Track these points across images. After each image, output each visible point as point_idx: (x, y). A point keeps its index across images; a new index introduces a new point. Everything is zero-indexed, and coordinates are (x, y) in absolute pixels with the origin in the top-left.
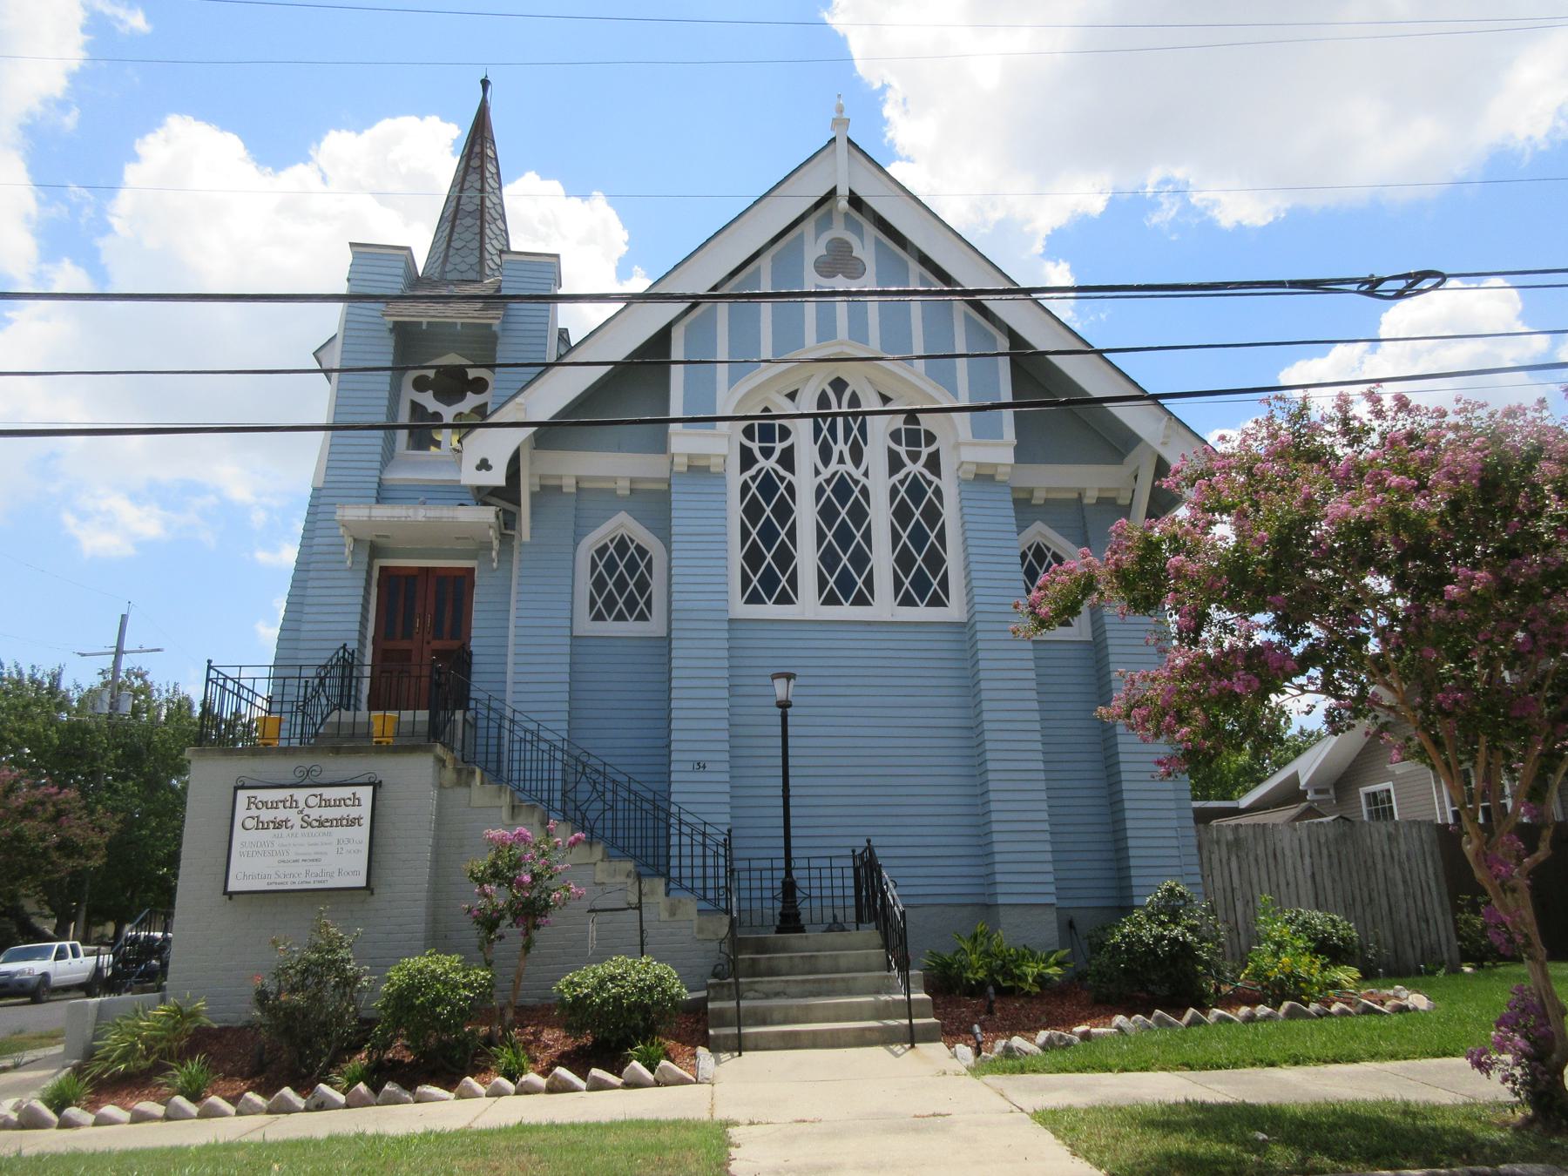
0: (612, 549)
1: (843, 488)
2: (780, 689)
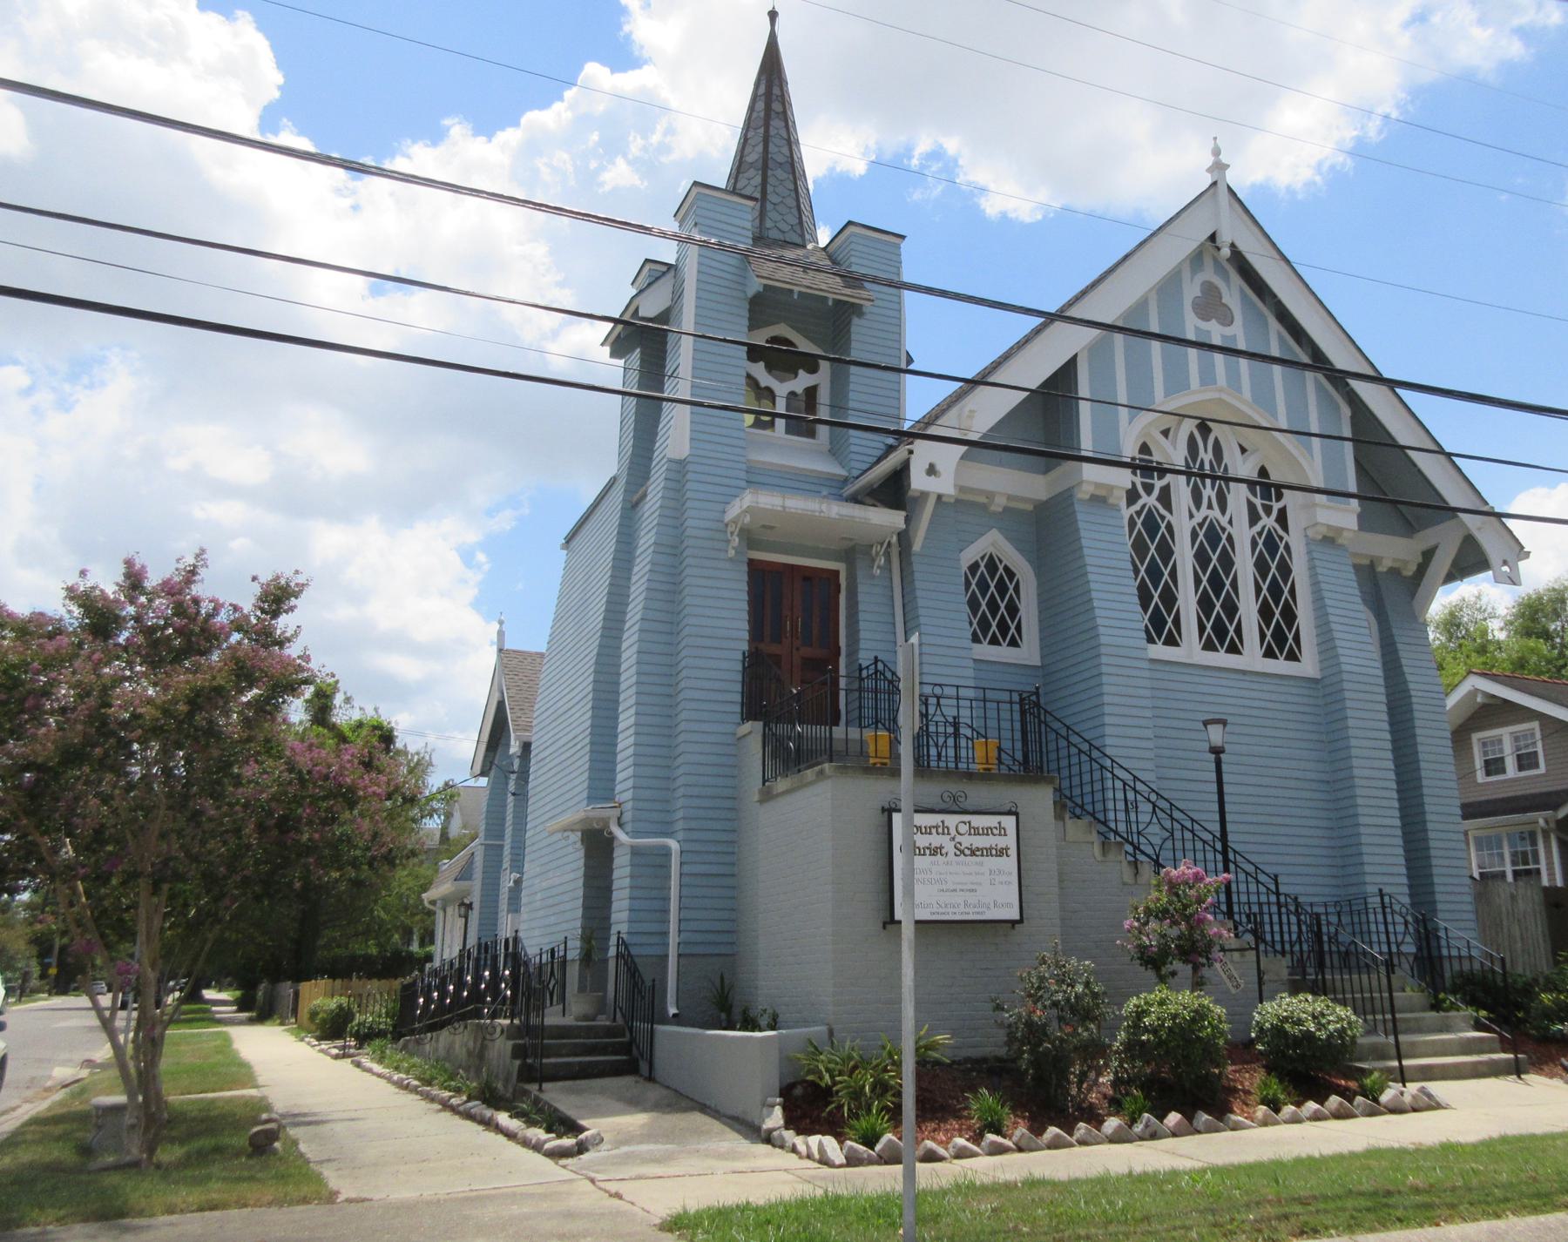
0: (982, 568)
1: (1213, 534)
2: (1216, 735)
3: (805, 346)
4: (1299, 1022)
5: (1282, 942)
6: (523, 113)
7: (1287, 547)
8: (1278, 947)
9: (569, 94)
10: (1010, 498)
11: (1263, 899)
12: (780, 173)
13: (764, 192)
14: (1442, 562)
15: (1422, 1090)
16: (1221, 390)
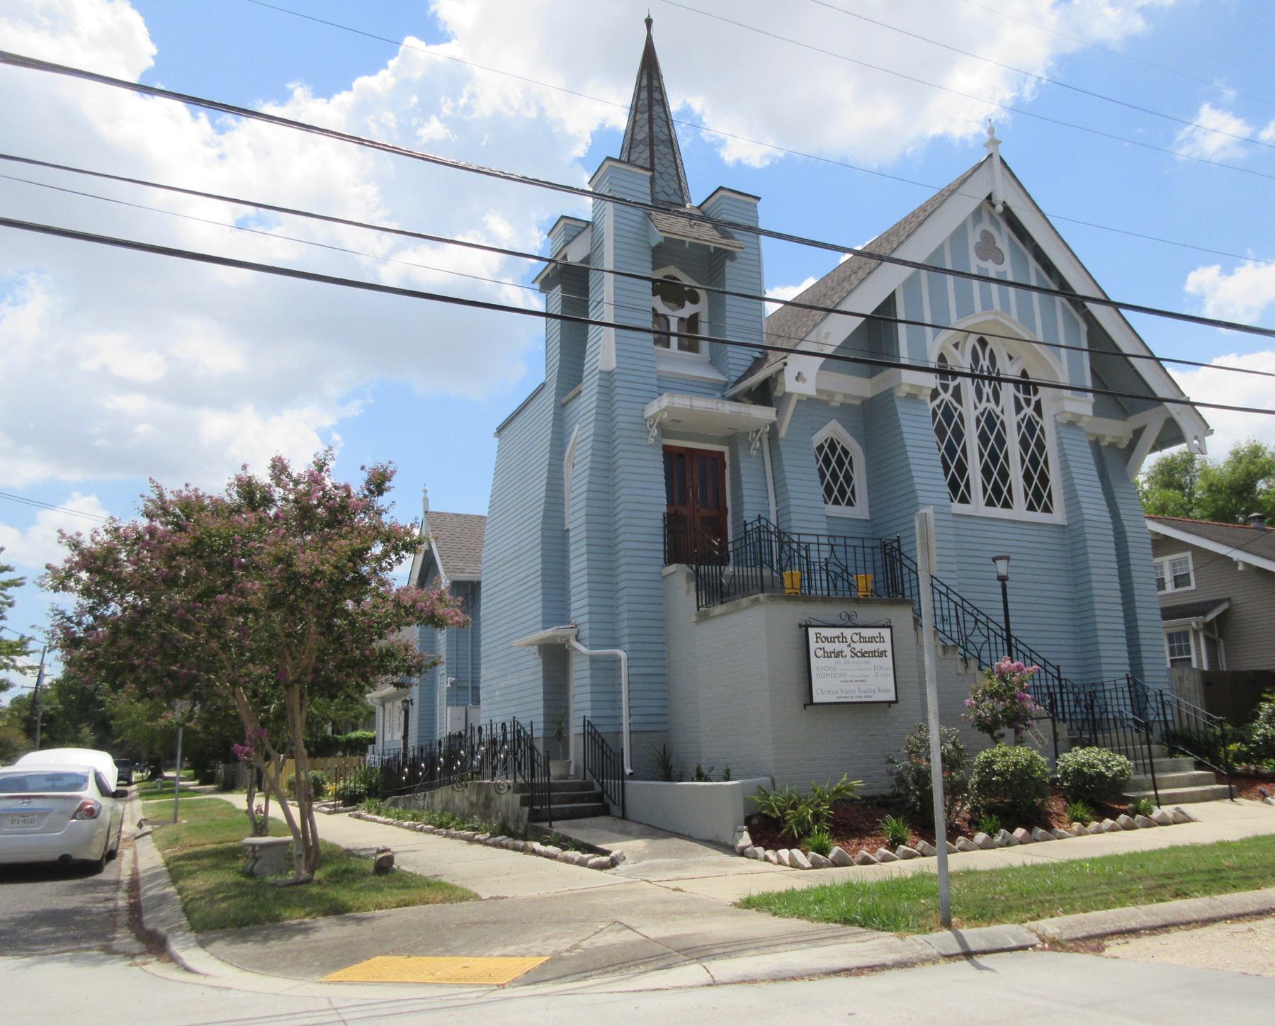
1: (991, 420)
2: (1002, 567)
3: (686, 280)
4: (1093, 766)
5: (1063, 713)
6: (353, 79)
7: (1042, 430)
8: (1061, 716)
9: (391, 63)
10: (845, 396)
11: (1050, 683)
12: (663, 149)
13: (652, 163)
14: (1150, 436)
15: (1177, 809)
16: (996, 313)
